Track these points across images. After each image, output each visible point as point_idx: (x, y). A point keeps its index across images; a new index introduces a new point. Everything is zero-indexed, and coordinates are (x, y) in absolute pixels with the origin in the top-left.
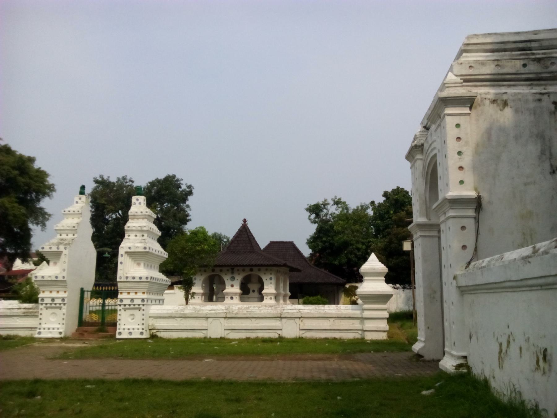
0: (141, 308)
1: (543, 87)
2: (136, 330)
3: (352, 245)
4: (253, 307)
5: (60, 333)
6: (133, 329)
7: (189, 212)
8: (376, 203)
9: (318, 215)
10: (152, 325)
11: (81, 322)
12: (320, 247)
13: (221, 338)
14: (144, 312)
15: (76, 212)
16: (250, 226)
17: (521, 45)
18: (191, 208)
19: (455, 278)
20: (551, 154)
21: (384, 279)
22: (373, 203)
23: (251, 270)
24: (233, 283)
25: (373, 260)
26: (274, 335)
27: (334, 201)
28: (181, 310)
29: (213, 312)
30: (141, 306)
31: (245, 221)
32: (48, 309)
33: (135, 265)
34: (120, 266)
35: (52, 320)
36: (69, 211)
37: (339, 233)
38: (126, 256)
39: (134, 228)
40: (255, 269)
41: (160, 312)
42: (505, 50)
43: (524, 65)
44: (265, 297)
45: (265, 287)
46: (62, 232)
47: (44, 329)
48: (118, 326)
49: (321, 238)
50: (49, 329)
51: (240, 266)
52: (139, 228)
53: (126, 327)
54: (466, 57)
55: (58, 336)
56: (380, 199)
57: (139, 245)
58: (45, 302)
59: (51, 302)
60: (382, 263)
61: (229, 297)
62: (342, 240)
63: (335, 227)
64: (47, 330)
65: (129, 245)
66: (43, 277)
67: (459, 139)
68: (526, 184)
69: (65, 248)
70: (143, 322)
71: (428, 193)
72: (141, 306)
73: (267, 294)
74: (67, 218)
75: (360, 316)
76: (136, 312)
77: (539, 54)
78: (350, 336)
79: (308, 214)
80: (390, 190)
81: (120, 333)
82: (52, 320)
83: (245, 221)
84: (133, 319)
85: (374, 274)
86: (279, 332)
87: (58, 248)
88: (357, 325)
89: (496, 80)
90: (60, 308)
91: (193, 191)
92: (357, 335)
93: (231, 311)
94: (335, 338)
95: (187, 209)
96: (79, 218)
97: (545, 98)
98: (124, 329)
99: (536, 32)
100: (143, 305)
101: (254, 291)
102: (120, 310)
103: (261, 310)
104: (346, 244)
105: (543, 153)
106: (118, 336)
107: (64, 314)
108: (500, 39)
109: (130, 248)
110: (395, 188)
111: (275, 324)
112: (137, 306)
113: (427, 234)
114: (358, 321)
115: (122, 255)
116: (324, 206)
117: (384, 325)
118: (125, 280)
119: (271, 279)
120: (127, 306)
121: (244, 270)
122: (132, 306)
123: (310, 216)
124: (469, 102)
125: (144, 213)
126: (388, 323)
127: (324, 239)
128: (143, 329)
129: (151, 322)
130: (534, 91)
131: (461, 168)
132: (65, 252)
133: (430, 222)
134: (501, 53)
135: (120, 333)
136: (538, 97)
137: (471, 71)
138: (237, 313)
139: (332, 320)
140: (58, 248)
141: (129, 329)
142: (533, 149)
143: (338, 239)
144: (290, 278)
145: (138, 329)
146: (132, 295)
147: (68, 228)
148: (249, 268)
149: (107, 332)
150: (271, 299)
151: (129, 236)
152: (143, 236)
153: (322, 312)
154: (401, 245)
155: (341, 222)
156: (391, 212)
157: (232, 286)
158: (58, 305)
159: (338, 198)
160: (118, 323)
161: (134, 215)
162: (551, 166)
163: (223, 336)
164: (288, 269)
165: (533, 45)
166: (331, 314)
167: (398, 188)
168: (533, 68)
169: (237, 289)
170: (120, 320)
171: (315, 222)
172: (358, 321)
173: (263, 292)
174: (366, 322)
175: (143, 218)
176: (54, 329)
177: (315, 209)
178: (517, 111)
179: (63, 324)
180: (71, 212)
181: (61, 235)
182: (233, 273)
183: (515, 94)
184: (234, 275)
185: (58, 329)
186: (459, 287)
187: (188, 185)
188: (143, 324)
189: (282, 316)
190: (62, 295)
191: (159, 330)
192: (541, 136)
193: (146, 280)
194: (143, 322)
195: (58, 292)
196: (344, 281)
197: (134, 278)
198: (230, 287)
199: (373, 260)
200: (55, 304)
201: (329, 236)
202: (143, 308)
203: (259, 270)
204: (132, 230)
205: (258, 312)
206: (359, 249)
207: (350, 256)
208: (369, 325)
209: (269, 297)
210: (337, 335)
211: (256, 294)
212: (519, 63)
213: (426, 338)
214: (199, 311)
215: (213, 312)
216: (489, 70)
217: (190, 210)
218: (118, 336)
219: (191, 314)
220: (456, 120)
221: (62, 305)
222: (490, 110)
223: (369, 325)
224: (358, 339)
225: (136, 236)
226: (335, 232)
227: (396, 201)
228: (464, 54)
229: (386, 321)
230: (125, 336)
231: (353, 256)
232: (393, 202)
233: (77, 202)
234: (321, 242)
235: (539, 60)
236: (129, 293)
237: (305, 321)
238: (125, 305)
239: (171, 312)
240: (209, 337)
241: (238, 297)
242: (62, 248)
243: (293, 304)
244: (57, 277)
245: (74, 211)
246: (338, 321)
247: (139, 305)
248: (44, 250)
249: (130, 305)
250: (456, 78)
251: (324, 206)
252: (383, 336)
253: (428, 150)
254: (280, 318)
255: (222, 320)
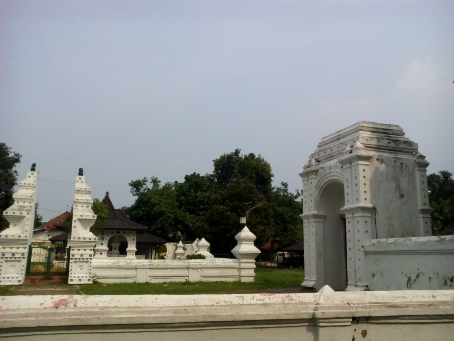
0: (88, 261)
1: (395, 155)
2: (15, 279)
3: (165, 214)
4: (122, 261)
5: (19, 281)
6: (82, 277)
7: (17, 177)
8: (179, 182)
9: (138, 190)
10: (94, 274)
11: (28, 273)
12: (141, 215)
13: (146, 282)
14: (90, 264)
15: (31, 185)
16: (111, 198)
17: (385, 131)
18: (18, 174)
19: (363, 247)
20: (400, 189)
21: (253, 243)
22: (176, 182)
23: (118, 232)
24: (103, 242)
25: (246, 231)
26: (183, 280)
27: (152, 179)
28: (116, 263)
29: (141, 264)
30: (89, 260)
31: (107, 193)
32: (8, 262)
33: (83, 229)
34: (73, 229)
35: (11, 271)
36: (25, 184)
37: (156, 204)
38: (77, 222)
39: (81, 201)
40: (121, 232)
41: (100, 264)
42: (378, 132)
43: (389, 143)
44: (128, 254)
45: (129, 246)
46: (20, 200)
47: (4, 278)
48: (70, 275)
49: (141, 207)
50: (8, 278)
51: (109, 229)
52: (86, 201)
53: (77, 275)
54: (363, 133)
55: (17, 283)
56: (182, 180)
57: (88, 214)
58: (6, 256)
59: (11, 256)
60: (253, 233)
61: (99, 253)
62: (159, 210)
63: (152, 200)
64: (6, 279)
65: (80, 213)
66: (6, 236)
67: (364, 177)
68: (390, 202)
69: (28, 214)
70: (90, 271)
71: (319, 199)
72: (89, 260)
73: (130, 251)
74: (22, 189)
75: (238, 267)
76: (84, 264)
77: (392, 137)
78: (231, 280)
79: (130, 188)
80: (189, 174)
81: (72, 280)
82: (11, 271)
83: (107, 193)
84: (81, 269)
85: (248, 240)
86: (187, 278)
87: (21, 213)
88: (236, 272)
89: (377, 148)
90: (19, 261)
91: (21, 159)
92: (236, 279)
93: (153, 264)
94: (222, 282)
95: (14, 174)
96: (33, 189)
97: (398, 160)
98: (75, 277)
99: (390, 125)
100: (91, 259)
101: (115, 249)
102: (72, 263)
103: (174, 263)
104: (161, 214)
105: (397, 187)
106: (70, 283)
107: (23, 266)
108: (375, 126)
109: (82, 216)
110: (193, 173)
111: (184, 272)
112: (85, 260)
113: (318, 220)
114: (237, 270)
115: (75, 221)
116: (144, 183)
117: (252, 273)
118: (78, 240)
119: (134, 240)
120: (78, 260)
121: (112, 232)
122: (81, 260)
123: (131, 190)
124: (368, 158)
125: (87, 190)
126: (255, 271)
127: (143, 208)
128: (90, 277)
129: (93, 271)
130: (393, 156)
131: (365, 192)
132: (27, 216)
133: (319, 214)
134: (379, 134)
135: (72, 280)
136: (395, 159)
137: (367, 142)
138: (158, 265)
139: (220, 269)
140: (21, 213)
141: (79, 277)
142: (393, 185)
143: (156, 209)
144: (137, 238)
145: (86, 277)
146: (82, 252)
147: (26, 198)
148: (116, 231)
149: (52, 279)
150: (133, 254)
151: (77, 206)
152: (88, 207)
153: (215, 264)
154: (239, 219)
155: (157, 196)
156: (192, 191)
157: (102, 244)
158: (17, 259)
159: (155, 177)
160: (70, 273)
161: (79, 191)
162: (400, 194)
163: (147, 281)
164: (135, 232)
165: (390, 132)
166: (220, 265)
167: (195, 173)
168: (392, 144)
169: (105, 247)
170: (71, 270)
171: (137, 195)
172: (236, 270)
173: (128, 249)
174: (242, 270)
175: (86, 193)
176: (13, 278)
177: (137, 185)
178: (387, 166)
179: (22, 274)
180: (27, 185)
181: (18, 202)
182: (103, 234)
183: (387, 157)
184: (104, 236)
185: (17, 278)
186: (365, 252)
187: (16, 153)
188: (90, 273)
189: (190, 267)
190: (21, 250)
191: (99, 277)
192: (396, 179)
193: (94, 241)
194: (90, 271)
195: (18, 248)
196: (165, 241)
197: (85, 238)
198: (100, 245)
199: (246, 231)
200: (15, 258)
201: (146, 206)
202: (90, 261)
203: (125, 233)
204: (80, 202)
205: (172, 264)
206: (169, 217)
207: (163, 223)
208: (244, 273)
209: (132, 253)
210: (223, 279)
211: (117, 251)
212: (387, 141)
213: (317, 279)
214: (130, 264)
215: (141, 264)
216: (374, 143)
217: (18, 175)
218: (70, 283)
219: (125, 265)
220: (364, 167)
221: (21, 259)
222: (376, 163)
223: (244, 273)
224: (236, 282)
225: (82, 207)
226: (152, 203)
227: (197, 183)
228: (361, 132)
229: (253, 270)
230: (76, 282)
231: (166, 222)
232: (194, 184)
233: (29, 177)
234: (141, 210)
235: (395, 141)
236: (79, 250)
237: (204, 270)
238: (76, 259)
239: (109, 264)
240: (137, 282)
241: (106, 253)
242: (24, 213)
243: (139, 258)
244: (19, 236)
245: (29, 184)
246: (224, 270)
247: (87, 259)
248: (8, 214)
249: (79, 259)
250: (361, 145)
251: (144, 183)
252: (252, 280)
253: (327, 174)
254: (188, 268)
255: (147, 270)
